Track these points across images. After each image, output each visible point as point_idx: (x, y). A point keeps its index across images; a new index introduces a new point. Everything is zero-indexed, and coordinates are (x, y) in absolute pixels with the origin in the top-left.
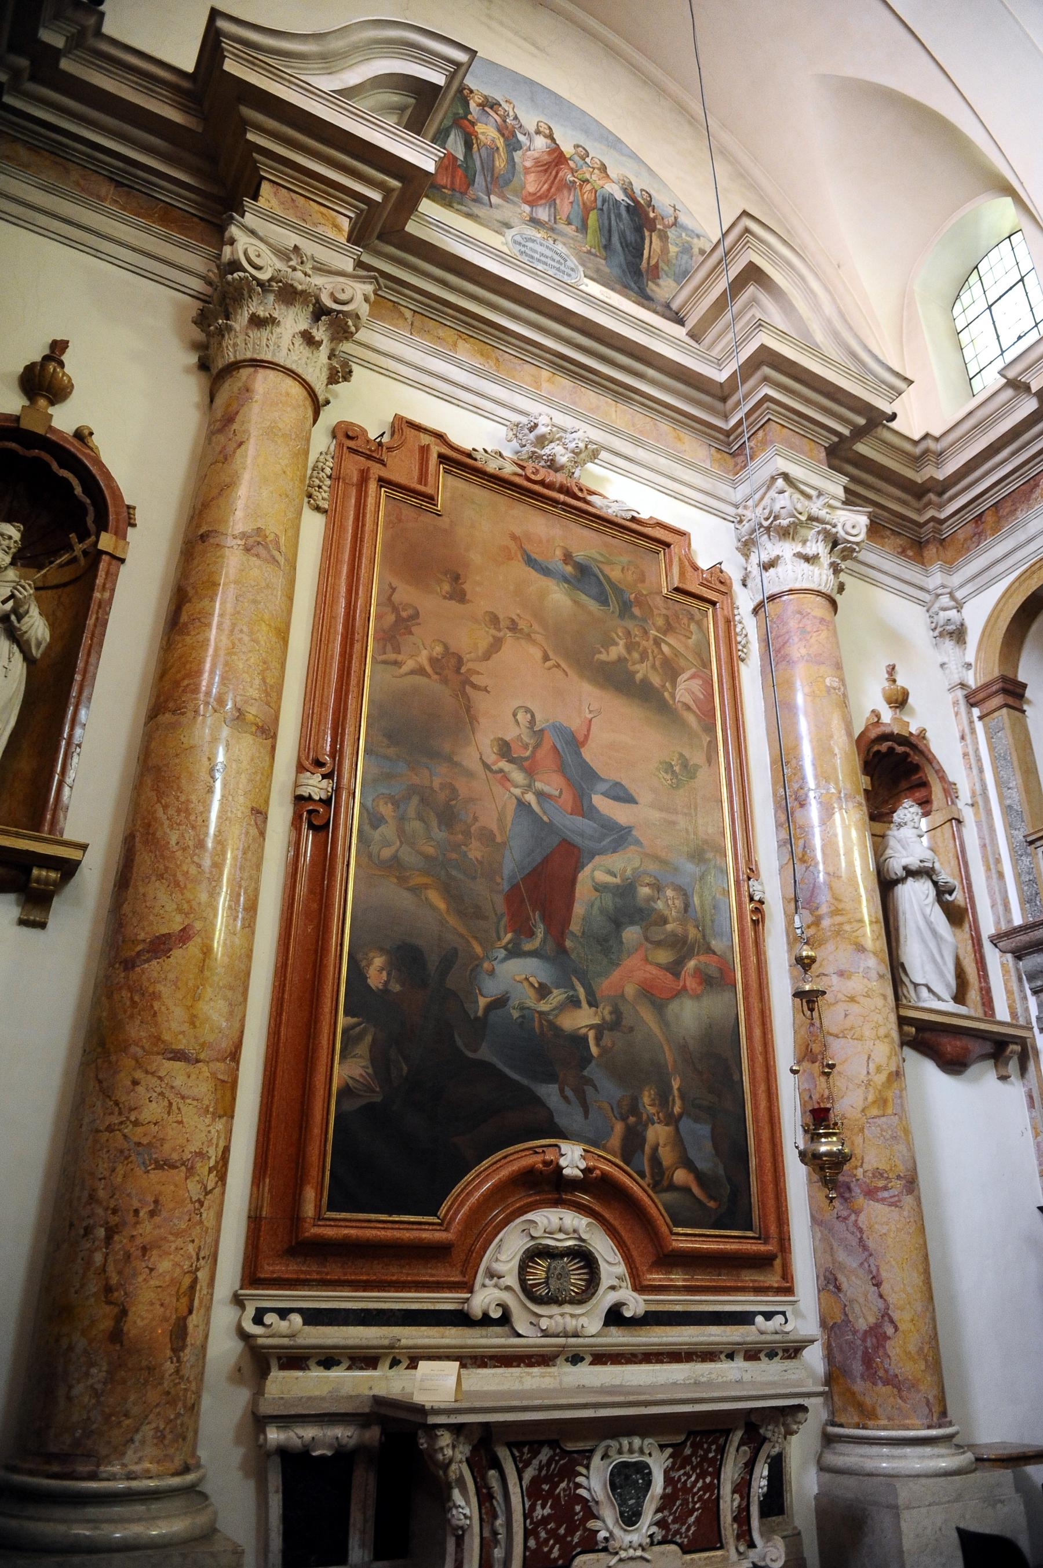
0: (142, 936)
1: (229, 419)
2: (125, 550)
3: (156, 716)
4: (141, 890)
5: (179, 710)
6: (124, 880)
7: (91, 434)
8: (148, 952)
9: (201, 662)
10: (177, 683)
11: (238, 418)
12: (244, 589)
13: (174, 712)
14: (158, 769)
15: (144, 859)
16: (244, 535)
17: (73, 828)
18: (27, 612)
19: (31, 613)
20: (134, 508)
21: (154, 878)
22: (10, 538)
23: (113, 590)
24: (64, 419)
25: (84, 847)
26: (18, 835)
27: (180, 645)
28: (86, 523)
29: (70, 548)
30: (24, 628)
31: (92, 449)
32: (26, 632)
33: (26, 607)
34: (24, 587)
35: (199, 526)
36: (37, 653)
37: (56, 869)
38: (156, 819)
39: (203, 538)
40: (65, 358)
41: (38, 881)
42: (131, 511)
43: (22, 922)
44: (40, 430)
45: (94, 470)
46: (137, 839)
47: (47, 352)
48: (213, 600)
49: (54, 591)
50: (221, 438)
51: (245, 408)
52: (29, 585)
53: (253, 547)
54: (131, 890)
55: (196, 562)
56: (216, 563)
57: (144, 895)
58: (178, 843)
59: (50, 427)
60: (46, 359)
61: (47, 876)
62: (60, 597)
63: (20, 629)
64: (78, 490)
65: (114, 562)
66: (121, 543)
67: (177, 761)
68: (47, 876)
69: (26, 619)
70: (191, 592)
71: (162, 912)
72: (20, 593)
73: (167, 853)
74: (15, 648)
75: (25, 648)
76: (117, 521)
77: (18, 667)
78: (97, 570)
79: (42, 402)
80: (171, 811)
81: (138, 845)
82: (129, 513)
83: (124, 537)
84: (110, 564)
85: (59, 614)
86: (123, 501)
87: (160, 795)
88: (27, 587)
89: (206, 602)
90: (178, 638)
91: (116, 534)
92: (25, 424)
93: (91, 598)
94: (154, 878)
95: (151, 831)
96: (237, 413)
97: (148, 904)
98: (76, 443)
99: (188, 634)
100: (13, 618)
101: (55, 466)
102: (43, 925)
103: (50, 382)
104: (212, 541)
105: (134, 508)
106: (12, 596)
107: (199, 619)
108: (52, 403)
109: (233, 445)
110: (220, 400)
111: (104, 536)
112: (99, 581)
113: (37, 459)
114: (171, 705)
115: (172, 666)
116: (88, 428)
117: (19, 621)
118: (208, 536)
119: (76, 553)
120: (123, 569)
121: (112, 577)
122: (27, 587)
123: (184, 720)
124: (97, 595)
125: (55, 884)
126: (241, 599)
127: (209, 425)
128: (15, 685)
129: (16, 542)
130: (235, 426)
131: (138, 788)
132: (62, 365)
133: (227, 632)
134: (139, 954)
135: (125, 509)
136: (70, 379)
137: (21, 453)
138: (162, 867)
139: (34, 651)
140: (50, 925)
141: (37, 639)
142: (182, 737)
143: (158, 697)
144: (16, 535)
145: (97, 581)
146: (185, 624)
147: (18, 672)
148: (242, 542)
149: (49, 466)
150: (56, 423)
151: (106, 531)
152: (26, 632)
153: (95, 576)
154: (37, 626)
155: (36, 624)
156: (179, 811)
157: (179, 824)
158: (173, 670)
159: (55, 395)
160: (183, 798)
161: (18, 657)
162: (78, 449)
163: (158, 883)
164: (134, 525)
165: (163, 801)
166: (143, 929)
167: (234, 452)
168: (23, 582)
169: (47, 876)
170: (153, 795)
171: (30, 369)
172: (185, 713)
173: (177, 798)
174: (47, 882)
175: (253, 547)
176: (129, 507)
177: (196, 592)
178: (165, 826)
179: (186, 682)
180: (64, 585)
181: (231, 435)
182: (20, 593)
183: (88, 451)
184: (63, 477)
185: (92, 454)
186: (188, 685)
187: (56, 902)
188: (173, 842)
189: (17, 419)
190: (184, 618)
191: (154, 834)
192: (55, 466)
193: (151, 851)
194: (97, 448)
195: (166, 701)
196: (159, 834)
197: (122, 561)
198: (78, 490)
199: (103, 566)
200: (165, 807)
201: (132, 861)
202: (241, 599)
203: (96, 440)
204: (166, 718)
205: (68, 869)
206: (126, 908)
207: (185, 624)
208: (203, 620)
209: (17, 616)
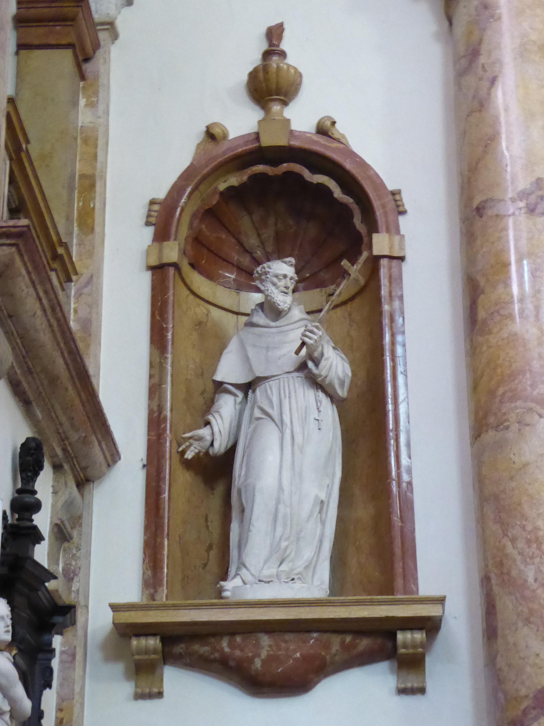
0: (523, 692)
1: (474, 53)
2: (402, 247)
3: (479, 436)
4: (511, 640)
5: (501, 425)
6: (490, 628)
7: (334, 123)
8: (534, 708)
9: (505, 250)
10: (492, 393)
11: (484, 48)
12: (539, 260)
13: (496, 428)
14: (497, 498)
15: (506, 604)
16: (523, 195)
17: (426, 587)
18: (322, 355)
19: (326, 355)
20: (399, 192)
21: (520, 624)
22: (285, 276)
23: (401, 298)
24: (301, 117)
25: (441, 601)
26: (372, 603)
27: (485, 348)
28: (354, 227)
29: (345, 274)
30: (324, 373)
31: (339, 141)
32: (326, 377)
33: (320, 349)
34: (311, 332)
35: (470, 199)
36: (342, 393)
37: (420, 629)
38: (506, 556)
39: (480, 210)
40: (284, 46)
41: (405, 646)
42: (397, 197)
43: (402, 691)
44: (282, 142)
45: (348, 165)
46: (493, 582)
47: (265, 46)
48: (507, 284)
49: (343, 308)
50: (470, 80)
51: (489, 32)
52: (317, 327)
53: (536, 204)
54: (500, 640)
55: (478, 242)
56: (500, 238)
57: (515, 645)
58: (536, 580)
59: (292, 132)
60: (267, 55)
61: (413, 638)
62: (350, 315)
63: (320, 376)
64: (337, 192)
65: (395, 263)
66: (397, 239)
67: (513, 484)
68: (413, 639)
69: (323, 363)
70: (482, 282)
71: (537, 661)
72: (310, 338)
73: (527, 593)
74: (321, 395)
75: (330, 391)
76: (385, 213)
77: (329, 413)
78: (379, 280)
79: (276, 108)
80: (521, 544)
81: (496, 589)
82: (396, 201)
83: (398, 231)
84: (390, 268)
85: (353, 333)
86: (385, 187)
87: (504, 526)
88: (316, 330)
89: (500, 289)
90: (480, 339)
91: (388, 231)
92: (266, 141)
93: (380, 313)
94: (520, 624)
95: (505, 571)
96: (480, 42)
97: (522, 655)
98: (322, 140)
99: (490, 332)
100: (310, 364)
101: (307, 174)
102: (422, 691)
103: (277, 83)
104: (490, 212)
105: (399, 192)
106: (303, 344)
107: (498, 312)
108: (285, 103)
109: (486, 84)
110: (460, 27)
111: (377, 238)
112: (384, 292)
113: (289, 174)
114: (492, 420)
115: (482, 376)
116: (329, 118)
117: (317, 365)
118: (484, 208)
119: (353, 276)
120: (406, 267)
121: (396, 280)
122: (316, 330)
123: (510, 435)
124: (386, 307)
125: (422, 645)
126: (538, 274)
127: (455, 63)
128: (331, 434)
129: (291, 278)
130: (482, 59)
131: (481, 520)
132: (283, 54)
133: (532, 319)
134: (525, 712)
135: (391, 197)
136: (295, 69)
137: (271, 174)
138: (526, 610)
139: (340, 392)
140: (429, 689)
141: (339, 378)
142: (512, 456)
143: (476, 413)
144: (290, 271)
145: (383, 293)
146: (484, 321)
147: (330, 419)
148: (522, 204)
149: (299, 177)
150: (296, 126)
151: (377, 231)
152: (326, 377)
153: (378, 288)
154: (336, 366)
155: (334, 363)
156: (529, 542)
157: (532, 558)
158: (485, 378)
159: (286, 95)
160: (529, 528)
161: (325, 401)
162: (325, 146)
163: (526, 629)
164: (403, 213)
165: (510, 534)
166: (523, 683)
167: (489, 94)
168: (310, 327)
169: (413, 639)
170: (495, 528)
171: (253, 76)
172: (507, 428)
173: (524, 528)
174: (414, 646)
175: (536, 204)
176: (393, 193)
177: (488, 281)
178: (519, 563)
179: (501, 390)
180: (352, 299)
181: (480, 72)
182: (310, 338)
183: (335, 145)
184: (318, 184)
185: (341, 146)
186: (504, 394)
187: (428, 660)
188: (531, 580)
189: (257, 136)
190: (482, 314)
191: (509, 573)
192: (307, 174)
193: (510, 594)
194: (343, 136)
195: (485, 416)
196: (514, 573)
197: (402, 259)
198: (337, 192)
199: (383, 272)
200: (513, 540)
201: (494, 606)
202: (538, 274)
203: (341, 128)
204: (490, 436)
205: (431, 626)
206: (500, 662)
207: (484, 321)
208: (502, 312)
209: (313, 361)
